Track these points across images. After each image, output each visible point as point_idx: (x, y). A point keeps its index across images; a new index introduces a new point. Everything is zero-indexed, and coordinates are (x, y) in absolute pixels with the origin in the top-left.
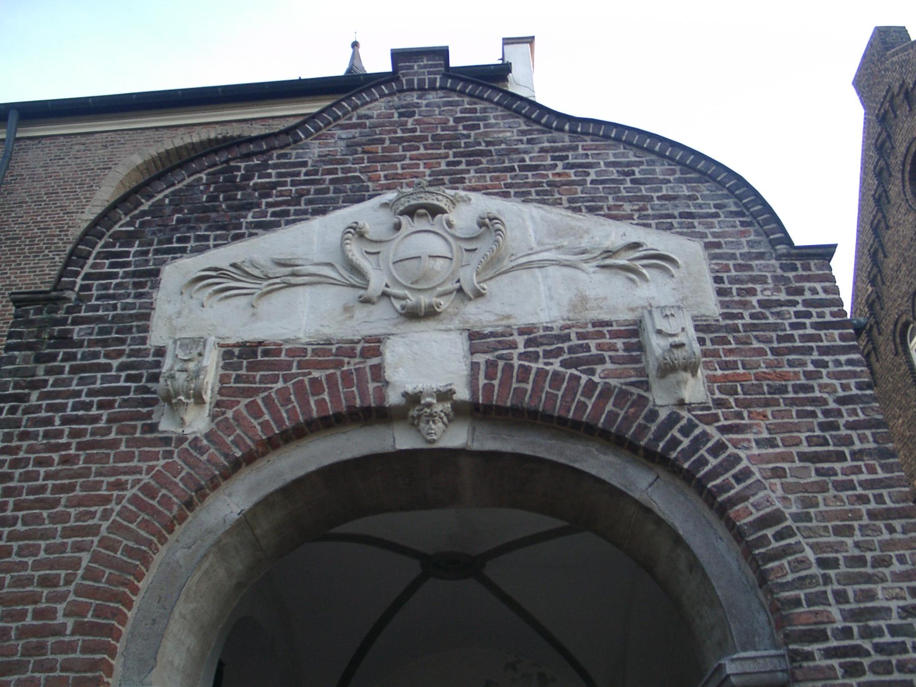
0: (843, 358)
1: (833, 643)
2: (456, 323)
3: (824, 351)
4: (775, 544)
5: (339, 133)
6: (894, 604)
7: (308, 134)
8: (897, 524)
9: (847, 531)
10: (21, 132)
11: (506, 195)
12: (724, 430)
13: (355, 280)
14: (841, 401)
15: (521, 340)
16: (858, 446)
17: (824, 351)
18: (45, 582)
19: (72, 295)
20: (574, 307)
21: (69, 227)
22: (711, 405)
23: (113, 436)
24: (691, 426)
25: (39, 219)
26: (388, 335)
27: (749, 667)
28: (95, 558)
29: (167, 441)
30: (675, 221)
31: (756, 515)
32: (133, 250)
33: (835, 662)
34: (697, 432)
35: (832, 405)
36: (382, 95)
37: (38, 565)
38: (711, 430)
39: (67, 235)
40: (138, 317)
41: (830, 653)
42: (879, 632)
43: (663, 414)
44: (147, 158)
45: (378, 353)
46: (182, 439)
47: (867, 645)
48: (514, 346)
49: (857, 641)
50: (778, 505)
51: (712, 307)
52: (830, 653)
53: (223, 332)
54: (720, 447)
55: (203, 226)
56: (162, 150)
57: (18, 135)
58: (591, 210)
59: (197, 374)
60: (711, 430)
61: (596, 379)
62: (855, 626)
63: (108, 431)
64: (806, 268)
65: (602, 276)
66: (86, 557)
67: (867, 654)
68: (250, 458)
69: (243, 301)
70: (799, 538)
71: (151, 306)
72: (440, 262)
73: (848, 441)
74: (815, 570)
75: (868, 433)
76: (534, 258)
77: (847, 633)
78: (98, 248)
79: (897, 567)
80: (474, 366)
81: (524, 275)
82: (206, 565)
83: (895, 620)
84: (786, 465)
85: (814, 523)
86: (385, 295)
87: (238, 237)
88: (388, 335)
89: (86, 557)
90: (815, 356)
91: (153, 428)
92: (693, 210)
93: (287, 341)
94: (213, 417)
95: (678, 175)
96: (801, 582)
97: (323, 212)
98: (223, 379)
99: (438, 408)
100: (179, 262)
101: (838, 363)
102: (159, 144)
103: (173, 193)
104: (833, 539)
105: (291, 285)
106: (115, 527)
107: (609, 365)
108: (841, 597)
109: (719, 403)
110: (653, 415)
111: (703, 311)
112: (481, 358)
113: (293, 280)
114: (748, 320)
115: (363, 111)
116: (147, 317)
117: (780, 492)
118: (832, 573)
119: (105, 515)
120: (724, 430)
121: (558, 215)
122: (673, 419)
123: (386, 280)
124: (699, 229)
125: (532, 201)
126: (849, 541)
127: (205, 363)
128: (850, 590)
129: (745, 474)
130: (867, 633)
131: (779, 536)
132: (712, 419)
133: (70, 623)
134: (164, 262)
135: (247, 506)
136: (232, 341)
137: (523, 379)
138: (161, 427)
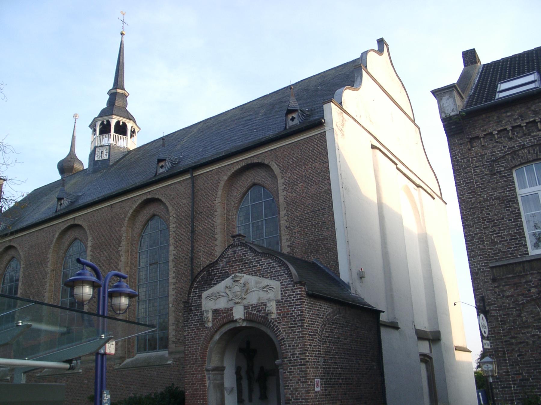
0: (299, 306)
1: (288, 359)
2: (242, 304)
3: (296, 305)
4: (283, 343)
5: (224, 259)
6: (298, 353)
7: (222, 258)
8: (301, 339)
9: (293, 341)
10: (194, 174)
11: (249, 274)
12: (278, 323)
13: (228, 296)
14: (297, 316)
15: (251, 307)
16: (298, 325)
17: (296, 305)
18: (196, 351)
19: (190, 301)
20: (258, 300)
21: (214, 206)
22: (497, 174)
23: (200, 327)
24: (273, 323)
25: (206, 205)
26: (233, 307)
27: (278, 362)
28: (201, 348)
29: (206, 328)
30: (276, 277)
31: (281, 338)
32: (197, 290)
33: (288, 362)
34: (274, 324)
35: (296, 317)
36: (230, 249)
37: (194, 349)
38: (276, 323)
39: (213, 209)
40: (199, 305)
41: (287, 361)
42: (295, 357)
43: (270, 320)
44: (228, 176)
45: (232, 310)
46: (208, 327)
47: (293, 359)
48: (249, 308)
49: (291, 359)
50: (284, 336)
51: (279, 298)
52: (287, 361)
53: (212, 307)
54: (277, 326)
55: (207, 284)
56: (231, 173)
57: (194, 175)
58: (263, 276)
59: (208, 317)
60: (276, 323)
61: (261, 314)
62: (292, 356)
63: (199, 327)
64: (297, 286)
65: (263, 293)
66: (199, 347)
67: (292, 361)
68: (218, 330)
69: (213, 301)
70: (286, 342)
71: (201, 303)
72: (239, 292)
73: (296, 324)
74: (288, 347)
75: (300, 322)
76: (253, 290)
77: (290, 357)
78: (192, 291)
79: (300, 346)
80: (244, 313)
81: (250, 293)
82: (216, 346)
83: (297, 355)
84: (286, 329)
85: (289, 339)
86: (232, 299)
87: (212, 287)
88: (233, 307)
89: (199, 347)
90: (295, 307)
91: (204, 326)
92: (279, 274)
93: (220, 309)
94: (212, 323)
95: (278, 265)
96: (285, 349)
97: (223, 280)
98: (213, 316)
99: (240, 321)
100: (204, 293)
101: (298, 308)
102: (230, 170)
103: (201, 277)
104: (291, 342)
105: (219, 298)
106: (202, 343)
107: (263, 312)
108: (290, 352)
109: (278, 318)
110: (268, 321)
111: (278, 298)
112: (246, 311)
113: (219, 296)
114: (285, 300)
115: (228, 253)
116: (201, 305)
117: (285, 334)
118: (290, 348)
119: (201, 341)
120: (278, 323)
121: (257, 278)
122: (271, 321)
123: (232, 296)
124: (280, 279)
125: (254, 275)
126: (293, 342)
127: (209, 315)
128: (292, 351)
129: (280, 331)
130: (293, 357)
131: (283, 342)
132: (276, 321)
133: (199, 357)
134: (202, 293)
135: (219, 337)
136: (213, 309)
137: (251, 315)
138: (206, 326)
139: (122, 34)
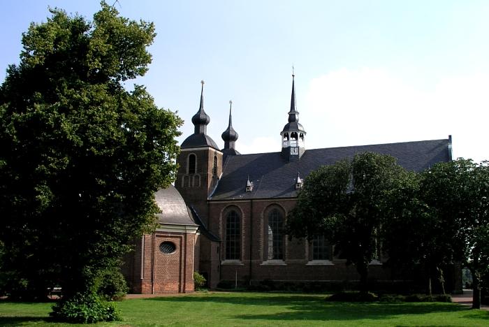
139: (293, 76)
